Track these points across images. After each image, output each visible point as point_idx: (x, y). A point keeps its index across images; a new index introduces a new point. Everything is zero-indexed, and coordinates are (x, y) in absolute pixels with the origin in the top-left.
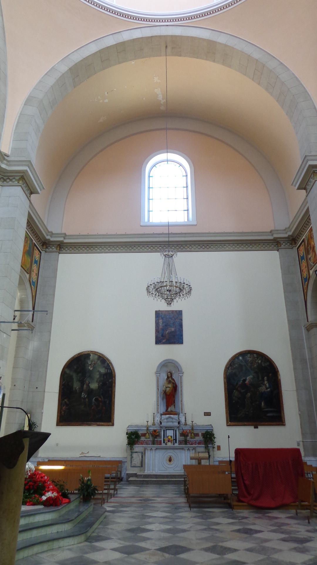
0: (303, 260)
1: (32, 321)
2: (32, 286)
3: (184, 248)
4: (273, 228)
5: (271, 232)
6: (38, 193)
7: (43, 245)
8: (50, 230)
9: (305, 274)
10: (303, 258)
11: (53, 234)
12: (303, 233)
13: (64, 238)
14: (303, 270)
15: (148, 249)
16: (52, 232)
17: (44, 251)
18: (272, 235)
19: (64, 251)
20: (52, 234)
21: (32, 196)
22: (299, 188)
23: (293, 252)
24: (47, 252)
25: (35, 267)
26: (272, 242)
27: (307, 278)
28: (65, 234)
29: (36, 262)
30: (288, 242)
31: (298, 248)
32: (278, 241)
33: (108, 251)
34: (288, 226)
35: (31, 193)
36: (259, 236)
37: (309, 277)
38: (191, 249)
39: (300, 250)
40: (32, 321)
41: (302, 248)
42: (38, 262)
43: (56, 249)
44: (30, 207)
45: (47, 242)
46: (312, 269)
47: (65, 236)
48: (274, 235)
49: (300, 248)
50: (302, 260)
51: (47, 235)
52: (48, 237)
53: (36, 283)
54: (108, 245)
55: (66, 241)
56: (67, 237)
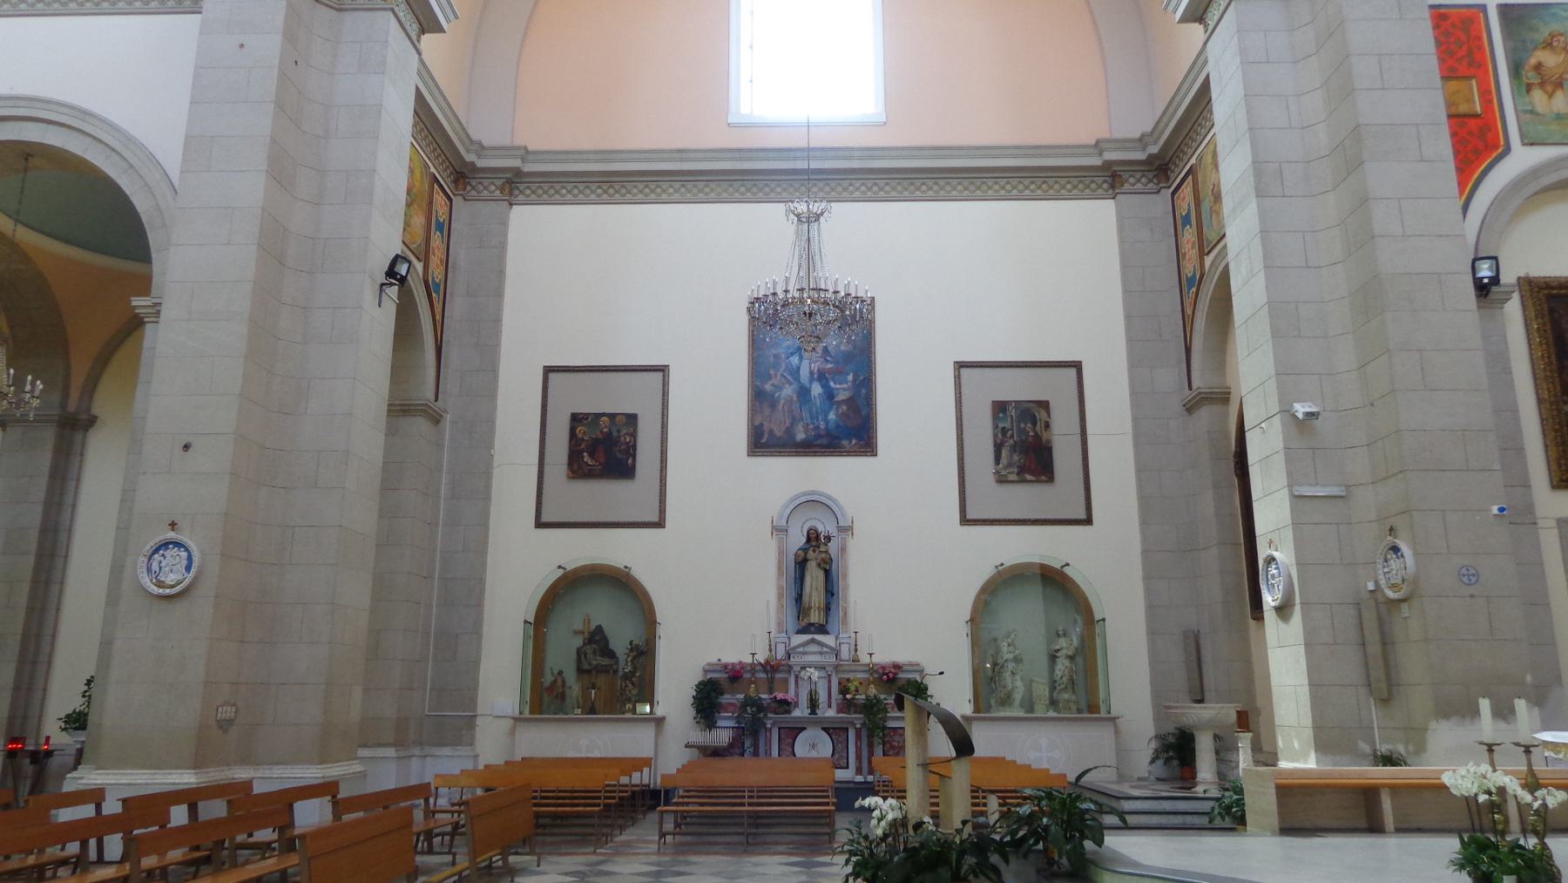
0: (1188, 227)
1: (436, 400)
2: (434, 295)
3: (629, 192)
4: (1106, 135)
5: (1141, 139)
6: (442, 31)
7: (456, 182)
8: (475, 136)
9: (1189, 268)
10: (1186, 220)
11: (483, 148)
12: (1189, 151)
13: (524, 160)
14: (1184, 254)
15: (599, 196)
16: (480, 144)
17: (460, 197)
18: (1101, 154)
19: (521, 197)
20: (481, 148)
21: (426, 38)
22: (1184, 19)
23: (1157, 205)
24: (469, 200)
25: (437, 240)
26: (1143, 168)
27: (1195, 277)
28: (526, 148)
29: (440, 226)
30: (1105, 181)
31: (1173, 194)
32: (1115, 171)
33: (572, 198)
34: (1148, 128)
35: (423, 31)
36: (1026, 156)
37: (1202, 276)
38: (1010, 192)
39: (1178, 198)
40: (436, 400)
41: (1187, 190)
42: (446, 228)
43: (501, 193)
44: (419, 74)
45: (1001, 708)
46: (1209, 252)
47: (526, 153)
48: (1104, 153)
49: (1180, 191)
50: (1184, 226)
51: (468, 151)
52: (469, 157)
53: (442, 288)
54: (681, 181)
55: (528, 168)
56: (531, 157)
